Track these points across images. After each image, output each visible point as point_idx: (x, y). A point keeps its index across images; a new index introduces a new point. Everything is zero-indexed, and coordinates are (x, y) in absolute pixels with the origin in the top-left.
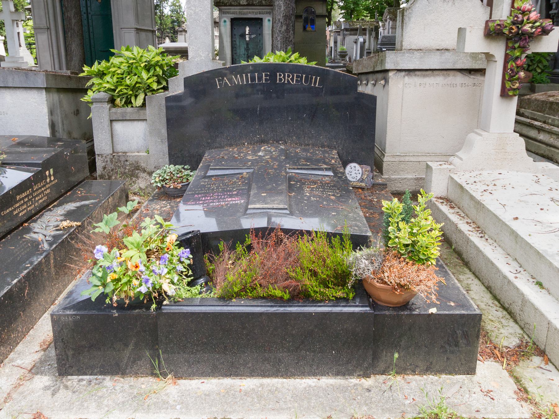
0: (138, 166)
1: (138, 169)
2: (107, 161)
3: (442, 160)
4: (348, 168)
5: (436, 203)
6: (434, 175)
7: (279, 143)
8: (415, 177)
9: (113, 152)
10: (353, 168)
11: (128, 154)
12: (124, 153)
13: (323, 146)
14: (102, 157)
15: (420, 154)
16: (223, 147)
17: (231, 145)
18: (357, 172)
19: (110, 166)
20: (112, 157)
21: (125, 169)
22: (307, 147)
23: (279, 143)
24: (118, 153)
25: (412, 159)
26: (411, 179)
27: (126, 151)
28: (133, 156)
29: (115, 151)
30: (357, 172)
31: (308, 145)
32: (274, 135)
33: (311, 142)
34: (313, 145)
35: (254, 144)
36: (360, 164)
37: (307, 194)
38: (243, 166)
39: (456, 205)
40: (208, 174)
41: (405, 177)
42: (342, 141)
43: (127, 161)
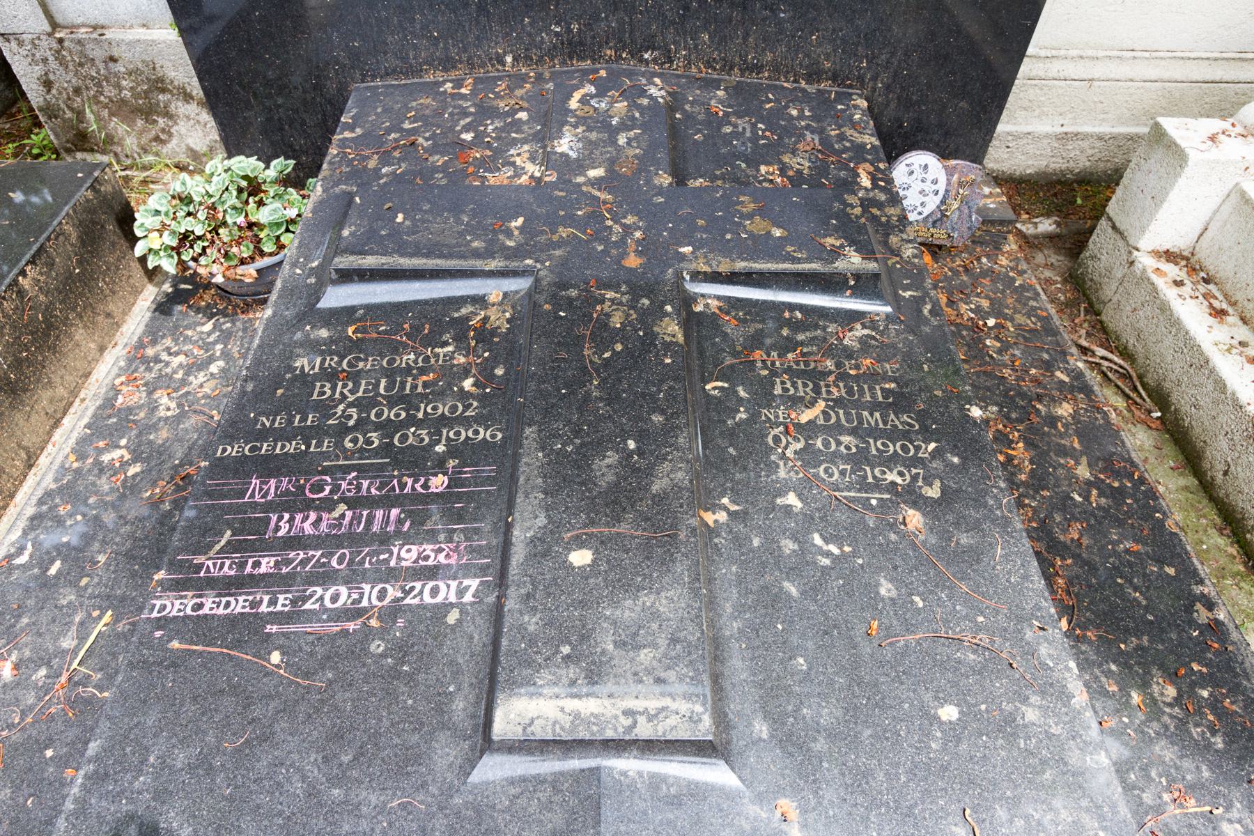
0: (161, 80)
1: (163, 90)
2: (45, 60)
3: (1166, 76)
4: (900, 173)
5: (1160, 282)
6: (1182, 182)
7: (641, 60)
8: (1060, 130)
9: (55, 25)
10: (918, 173)
11: (109, 35)
12: (95, 28)
13: (814, 75)
14: (21, 44)
15: (1101, 54)
16: (416, 71)
17: (448, 64)
18: (928, 187)
19: (65, 79)
20: (55, 46)
21: (119, 87)
22: (751, 79)
23: (641, 60)
24: (73, 28)
25: (1071, 70)
26: (1047, 136)
27: (102, 21)
28: (131, 44)
29: (59, 19)
30: (928, 187)
31: (758, 69)
32: (621, 23)
33: (769, 56)
34: (777, 70)
35: (540, 60)
36: (944, 155)
37: (792, 499)
38: (489, 254)
39: (1233, 304)
40: (324, 304)
41: (1029, 129)
42: (893, 54)
43: (113, 59)
